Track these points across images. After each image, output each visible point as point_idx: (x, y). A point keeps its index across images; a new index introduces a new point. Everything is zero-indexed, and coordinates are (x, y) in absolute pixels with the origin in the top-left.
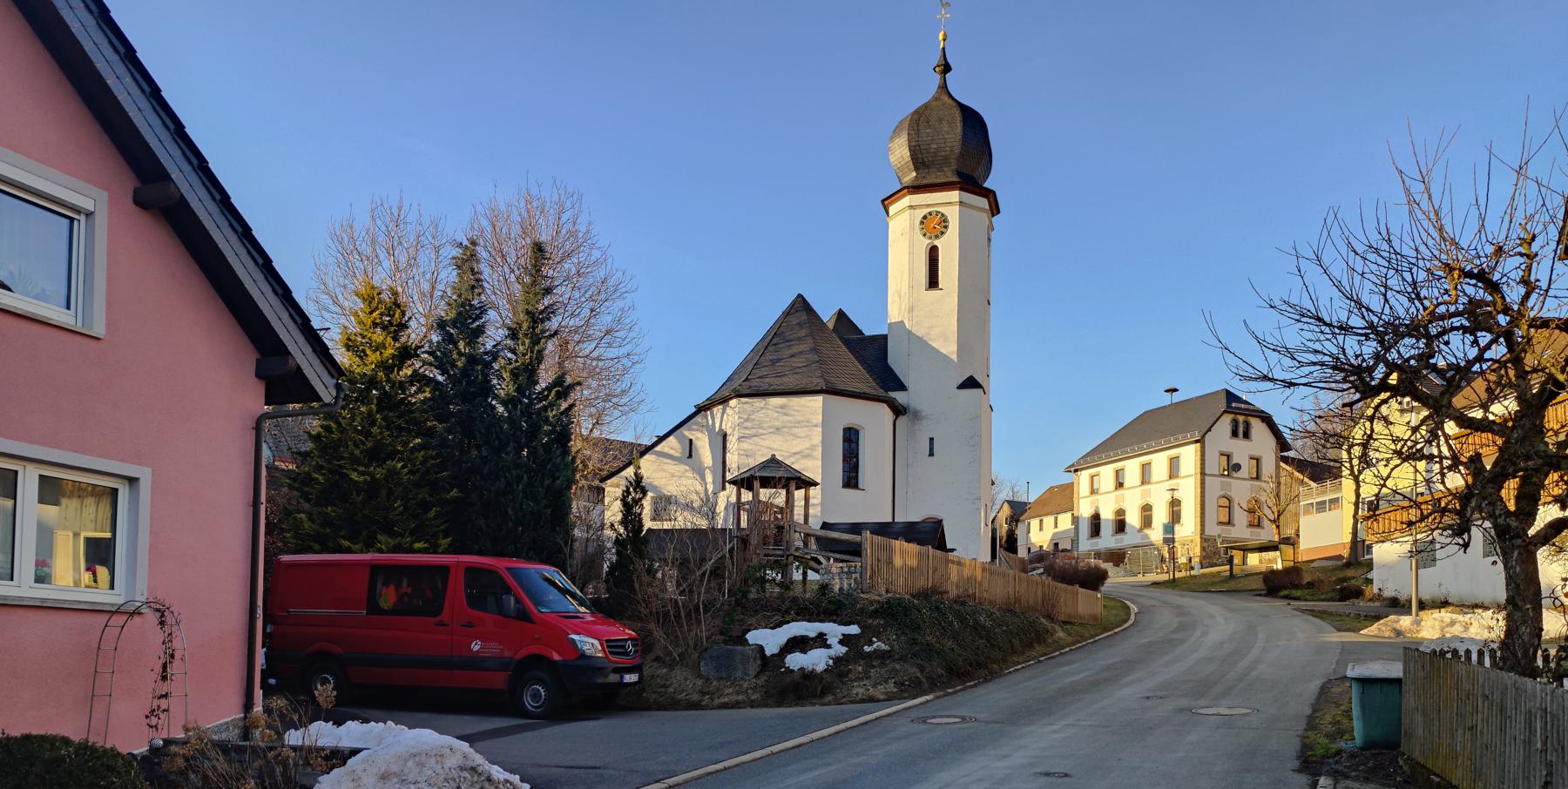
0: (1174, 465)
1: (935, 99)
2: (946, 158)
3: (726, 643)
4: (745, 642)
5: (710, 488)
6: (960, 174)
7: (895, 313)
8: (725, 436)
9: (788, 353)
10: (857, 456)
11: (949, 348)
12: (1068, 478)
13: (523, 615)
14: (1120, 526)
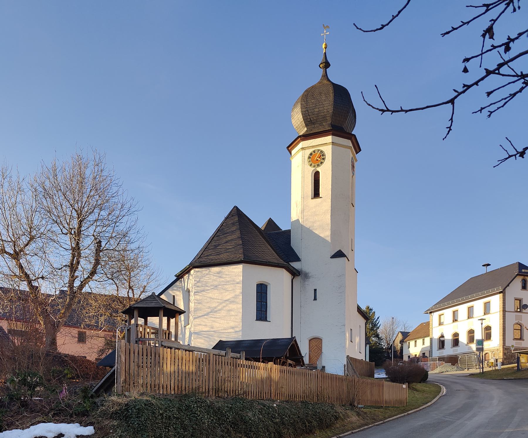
0: (487, 306)
1: (319, 83)
2: (324, 117)
8: (189, 292)
11: (326, 234)
12: (424, 319)
14: (456, 342)
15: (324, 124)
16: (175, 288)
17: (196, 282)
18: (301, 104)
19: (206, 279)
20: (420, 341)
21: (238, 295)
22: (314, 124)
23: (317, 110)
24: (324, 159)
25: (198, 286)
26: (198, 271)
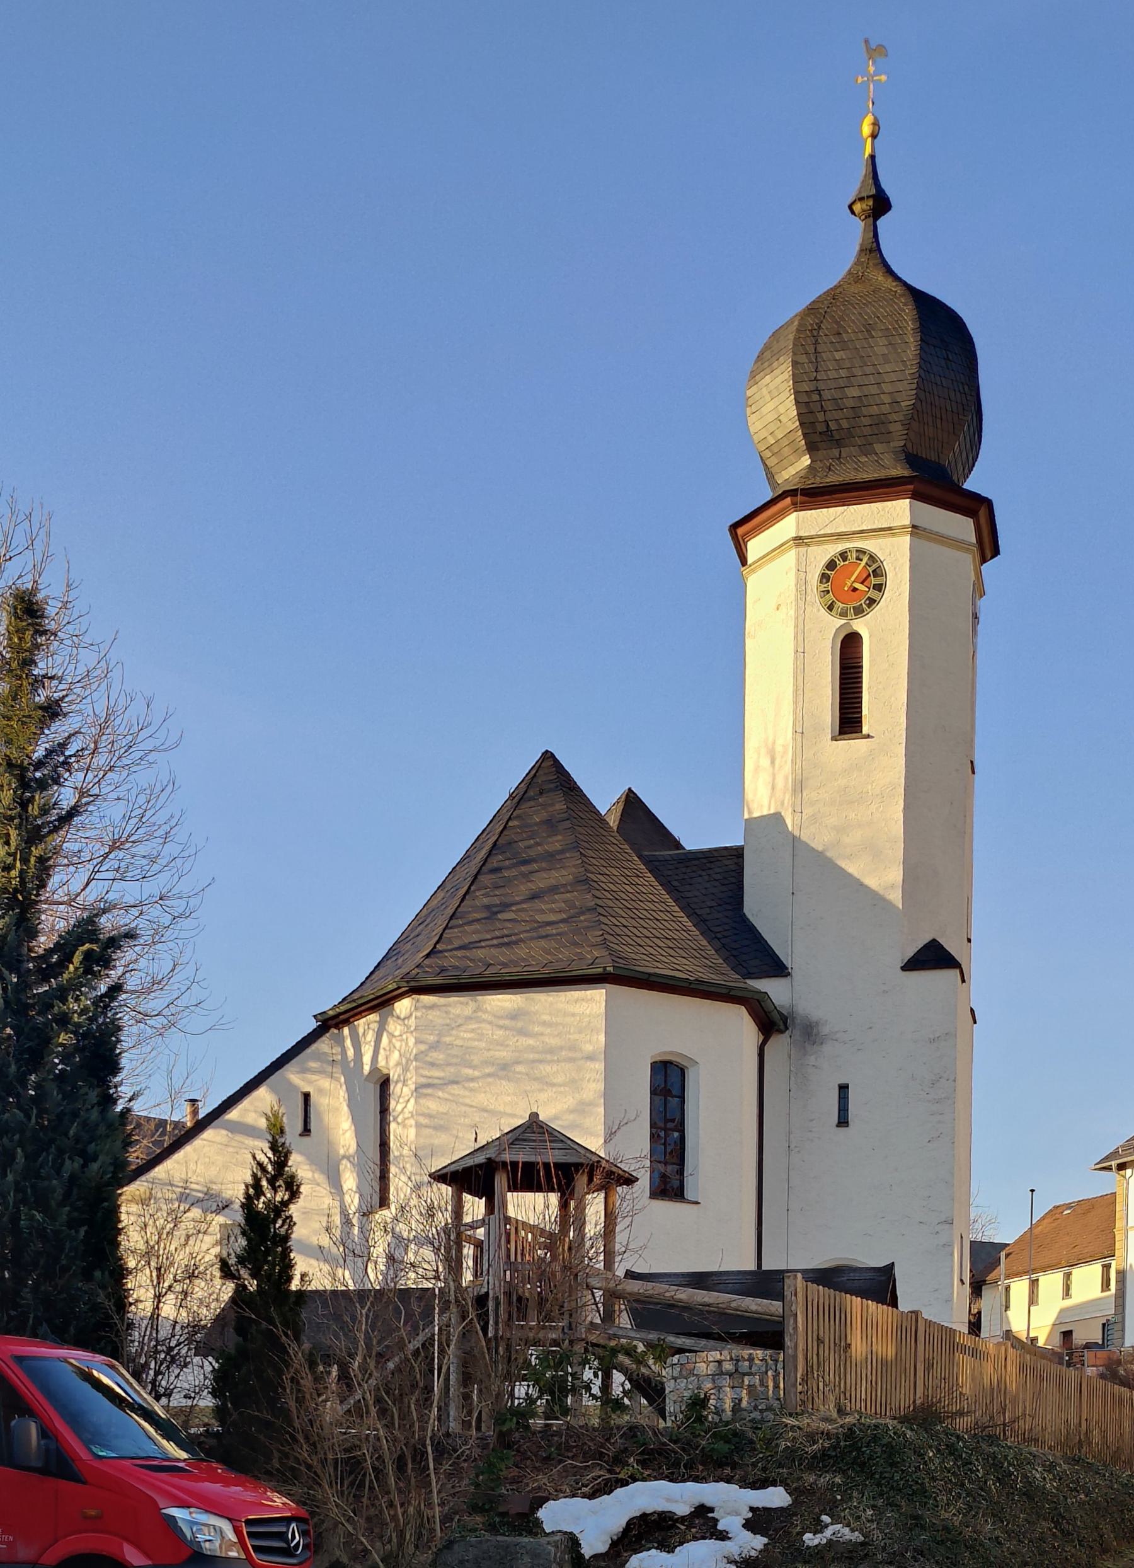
1: (855, 277)
3: (492, 1528)
4: (534, 1527)
5: (353, 1202)
6: (911, 459)
7: (762, 794)
9: (523, 889)
10: (681, 1128)
13: (58, 1465)
15: (878, 447)
16: (313, 1065)
17: (423, 1047)
18: (795, 364)
19: (464, 1036)
20: (1050, 1282)
21: (591, 1104)
22: (839, 443)
23: (854, 392)
24: (879, 588)
25: (432, 1064)
26: (432, 1007)
